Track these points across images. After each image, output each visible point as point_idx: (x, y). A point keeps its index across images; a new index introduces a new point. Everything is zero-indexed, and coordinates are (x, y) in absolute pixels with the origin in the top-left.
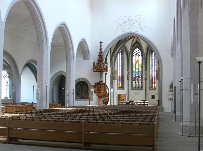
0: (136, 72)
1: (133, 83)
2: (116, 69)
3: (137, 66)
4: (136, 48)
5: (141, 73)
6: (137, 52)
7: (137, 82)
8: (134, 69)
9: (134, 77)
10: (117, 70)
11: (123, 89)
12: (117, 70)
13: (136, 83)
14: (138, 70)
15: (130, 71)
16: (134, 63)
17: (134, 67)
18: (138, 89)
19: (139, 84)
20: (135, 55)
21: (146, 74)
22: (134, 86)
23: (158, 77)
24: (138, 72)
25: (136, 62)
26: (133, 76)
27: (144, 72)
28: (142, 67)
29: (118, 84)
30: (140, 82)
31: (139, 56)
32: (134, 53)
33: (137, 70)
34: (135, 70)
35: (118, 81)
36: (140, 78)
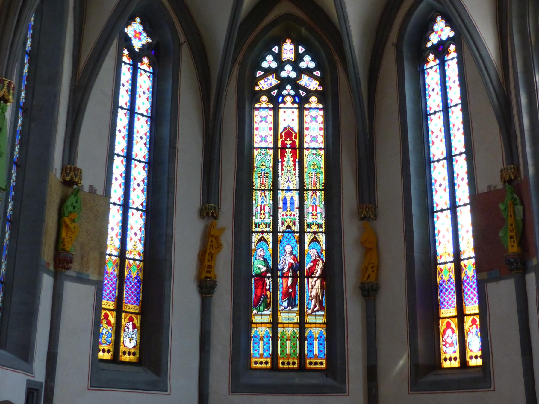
0: (275, 232)
1: (249, 324)
2: (89, 179)
3: (288, 177)
4: (280, 43)
5: (322, 238)
6: (288, 72)
7: (288, 316)
8: (261, 201)
9: (261, 277)
10: (100, 191)
11: (150, 376)
12: (100, 191)
13: (274, 324)
14: (296, 212)
15: (226, 218)
16: (262, 161)
17: (257, 182)
18: (297, 379)
19: (302, 338)
20: (268, 93)
21: (370, 248)
22: (260, 351)
23: (513, 248)
24: (296, 228)
25: (278, 151)
26: (250, 264)
27: (350, 231)
28: (331, 190)
29: (106, 331)
30: (310, 319)
31: (306, 100)
32: (259, 73)
33: (288, 217)
34: (269, 209)
35: (108, 304)
36: (314, 287)
